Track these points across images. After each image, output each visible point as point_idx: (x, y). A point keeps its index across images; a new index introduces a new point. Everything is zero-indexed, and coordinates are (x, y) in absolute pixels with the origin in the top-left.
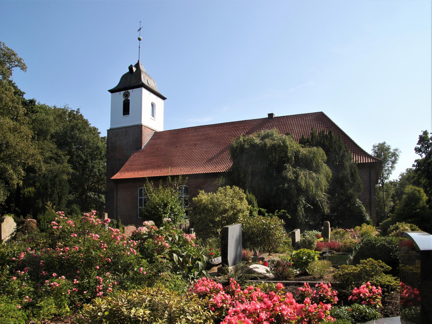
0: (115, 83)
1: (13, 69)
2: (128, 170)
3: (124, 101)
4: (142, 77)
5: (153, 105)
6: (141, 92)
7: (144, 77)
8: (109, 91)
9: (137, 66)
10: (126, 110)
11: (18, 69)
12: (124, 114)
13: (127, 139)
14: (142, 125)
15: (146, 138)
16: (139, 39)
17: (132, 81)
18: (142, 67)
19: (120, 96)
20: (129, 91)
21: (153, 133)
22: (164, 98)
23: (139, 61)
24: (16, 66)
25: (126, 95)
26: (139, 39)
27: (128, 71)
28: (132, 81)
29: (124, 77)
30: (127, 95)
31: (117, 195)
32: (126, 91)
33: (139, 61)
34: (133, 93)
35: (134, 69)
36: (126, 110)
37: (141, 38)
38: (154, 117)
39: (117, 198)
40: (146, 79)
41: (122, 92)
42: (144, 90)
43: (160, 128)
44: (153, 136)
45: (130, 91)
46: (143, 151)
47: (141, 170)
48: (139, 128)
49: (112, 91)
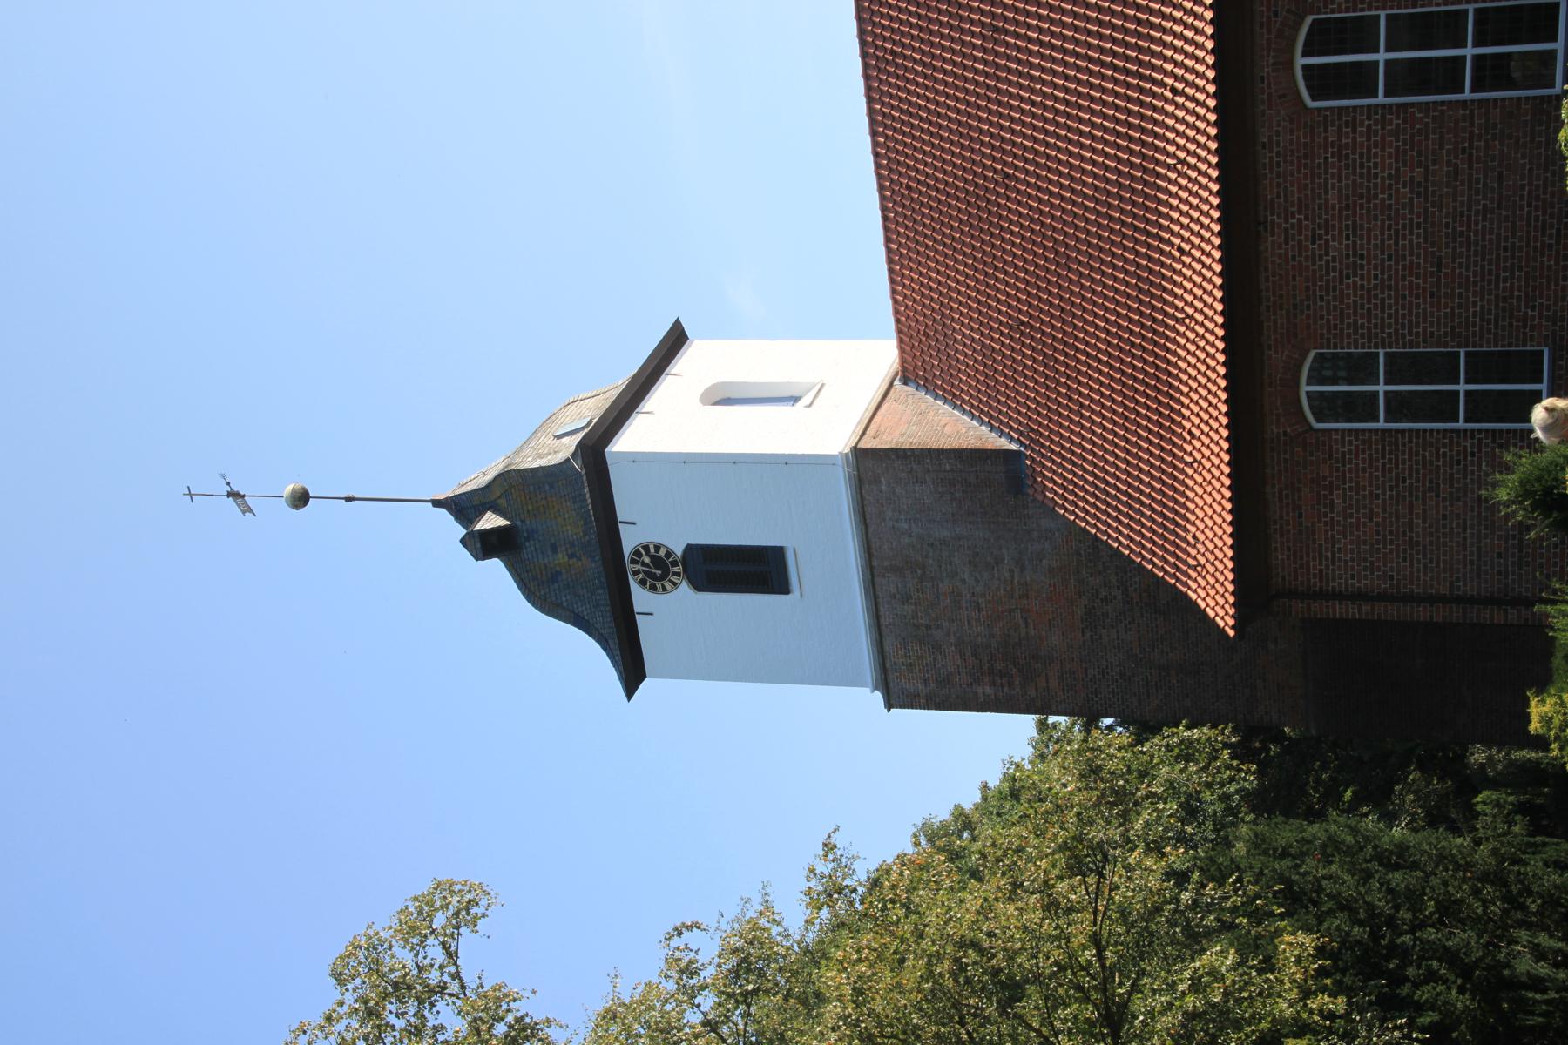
0: (581, 655)
1: (471, 981)
2: (1172, 522)
3: (699, 585)
4: (535, 465)
5: (724, 397)
6: (635, 458)
7: (541, 456)
8: (630, 692)
9: (463, 507)
10: (752, 570)
11: (467, 943)
12: (784, 588)
13: (961, 576)
14: (856, 451)
15: (947, 426)
16: (301, 499)
17: (565, 538)
18: (476, 475)
19: (664, 613)
20: (628, 548)
21: (910, 389)
22: (676, 340)
23: (437, 503)
24: (452, 955)
25: (658, 568)
26: (301, 499)
27: (496, 565)
28: (565, 538)
29: (545, 591)
30: (656, 561)
31: (1360, 596)
32: (630, 567)
33: (437, 503)
34: (645, 522)
35: (491, 521)
36: (752, 570)
37: (289, 488)
38: (802, 378)
39: (1382, 597)
40: (551, 441)
41: (641, 597)
42: (629, 441)
43: (885, 354)
44: (928, 385)
45: (630, 540)
46: (1028, 434)
47: (1167, 419)
48: (873, 468)
49: (632, 673)
